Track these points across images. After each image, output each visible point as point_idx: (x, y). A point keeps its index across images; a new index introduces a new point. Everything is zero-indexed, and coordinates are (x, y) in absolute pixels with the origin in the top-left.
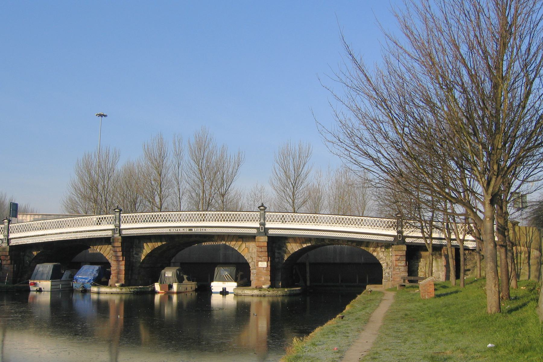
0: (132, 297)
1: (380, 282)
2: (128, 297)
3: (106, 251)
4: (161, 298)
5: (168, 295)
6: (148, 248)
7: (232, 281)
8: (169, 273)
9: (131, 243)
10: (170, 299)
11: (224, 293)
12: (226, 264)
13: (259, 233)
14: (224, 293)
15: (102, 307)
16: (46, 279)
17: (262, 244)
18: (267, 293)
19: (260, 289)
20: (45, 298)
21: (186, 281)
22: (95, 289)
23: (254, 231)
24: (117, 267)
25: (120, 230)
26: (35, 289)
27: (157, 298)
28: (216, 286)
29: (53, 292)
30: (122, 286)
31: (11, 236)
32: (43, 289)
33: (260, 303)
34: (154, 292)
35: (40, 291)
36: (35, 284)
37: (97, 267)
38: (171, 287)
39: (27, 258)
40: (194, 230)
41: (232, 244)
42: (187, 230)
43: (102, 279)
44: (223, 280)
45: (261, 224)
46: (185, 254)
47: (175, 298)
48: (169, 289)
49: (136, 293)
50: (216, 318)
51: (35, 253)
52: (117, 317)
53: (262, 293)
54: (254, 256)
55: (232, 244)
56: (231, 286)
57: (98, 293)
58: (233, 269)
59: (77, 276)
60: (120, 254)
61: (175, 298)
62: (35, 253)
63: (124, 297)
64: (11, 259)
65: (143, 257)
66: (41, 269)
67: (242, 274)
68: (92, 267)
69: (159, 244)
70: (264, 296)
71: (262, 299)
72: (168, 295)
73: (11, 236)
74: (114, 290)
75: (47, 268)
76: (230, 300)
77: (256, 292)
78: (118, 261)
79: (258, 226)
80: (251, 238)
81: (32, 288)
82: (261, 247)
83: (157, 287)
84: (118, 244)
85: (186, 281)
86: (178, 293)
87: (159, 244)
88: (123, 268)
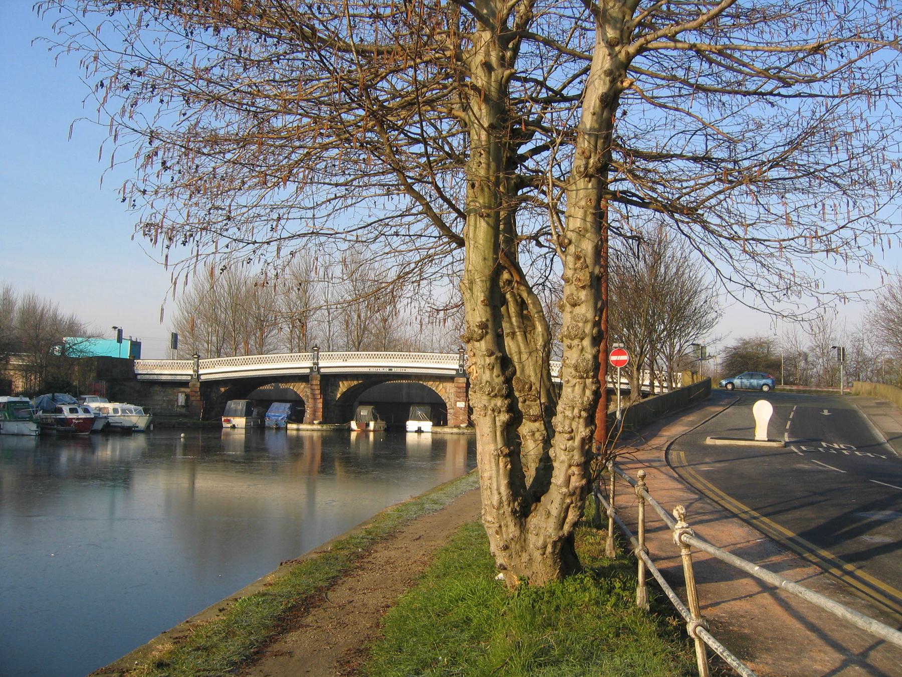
0: (332, 434)
1: (445, 424)
2: (328, 433)
3: (300, 389)
4: (358, 437)
5: (365, 431)
6: (343, 387)
7: (426, 420)
8: (364, 412)
9: (329, 381)
10: (367, 437)
11: (419, 431)
12: (421, 404)
13: (458, 375)
14: (419, 431)
15: (297, 443)
16: (241, 416)
17: (461, 385)
18: (466, 431)
19: (459, 427)
20: (240, 435)
21: (379, 420)
22: (292, 426)
23: (454, 372)
24: (313, 405)
25: (319, 368)
26: (229, 425)
27: (353, 435)
28: (411, 425)
29: (247, 428)
30: (319, 423)
31: (201, 372)
32: (237, 424)
33: (459, 440)
34: (350, 430)
35: (234, 427)
36: (229, 421)
37: (288, 405)
38: (368, 425)
39: (213, 395)
40: (394, 370)
41: (429, 384)
42: (387, 370)
43: (297, 416)
44: (418, 419)
45: (460, 366)
46: (375, 392)
47: (371, 435)
48: (364, 428)
49: (335, 430)
50: (410, 454)
51: (223, 390)
52: (312, 453)
53: (461, 431)
54: (452, 396)
55: (429, 384)
56: (427, 425)
57: (298, 430)
58: (429, 409)
59: (269, 413)
60: (318, 392)
61: (371, 435)
62: (223, 390)
63: (324, 433)
64: (201, 395)
65: (339, 395)
66: (233, 406)
67: (438, 413)
68: (283, 404)
69: (355, 383)
70: (463, 434)
71: (461, 437)
72: (365, 431)
73: (201, 372)
74: (315, 427)
75: (239, 405)
76: (427, 438)
77: (455, 430)
78: (315, 399)
79: (457, 367)
80: (451, 379)
81: (225, 425)
82: (460, 388)
83: (353, 425)
84: (316, 382)
85: (379, 420)
86: (374, 431)
87: (355, 383)
88: (320, 405)
